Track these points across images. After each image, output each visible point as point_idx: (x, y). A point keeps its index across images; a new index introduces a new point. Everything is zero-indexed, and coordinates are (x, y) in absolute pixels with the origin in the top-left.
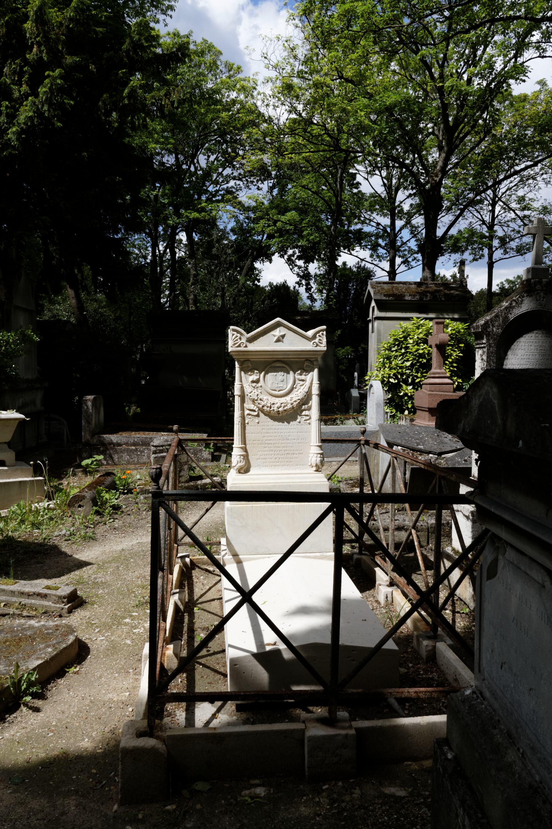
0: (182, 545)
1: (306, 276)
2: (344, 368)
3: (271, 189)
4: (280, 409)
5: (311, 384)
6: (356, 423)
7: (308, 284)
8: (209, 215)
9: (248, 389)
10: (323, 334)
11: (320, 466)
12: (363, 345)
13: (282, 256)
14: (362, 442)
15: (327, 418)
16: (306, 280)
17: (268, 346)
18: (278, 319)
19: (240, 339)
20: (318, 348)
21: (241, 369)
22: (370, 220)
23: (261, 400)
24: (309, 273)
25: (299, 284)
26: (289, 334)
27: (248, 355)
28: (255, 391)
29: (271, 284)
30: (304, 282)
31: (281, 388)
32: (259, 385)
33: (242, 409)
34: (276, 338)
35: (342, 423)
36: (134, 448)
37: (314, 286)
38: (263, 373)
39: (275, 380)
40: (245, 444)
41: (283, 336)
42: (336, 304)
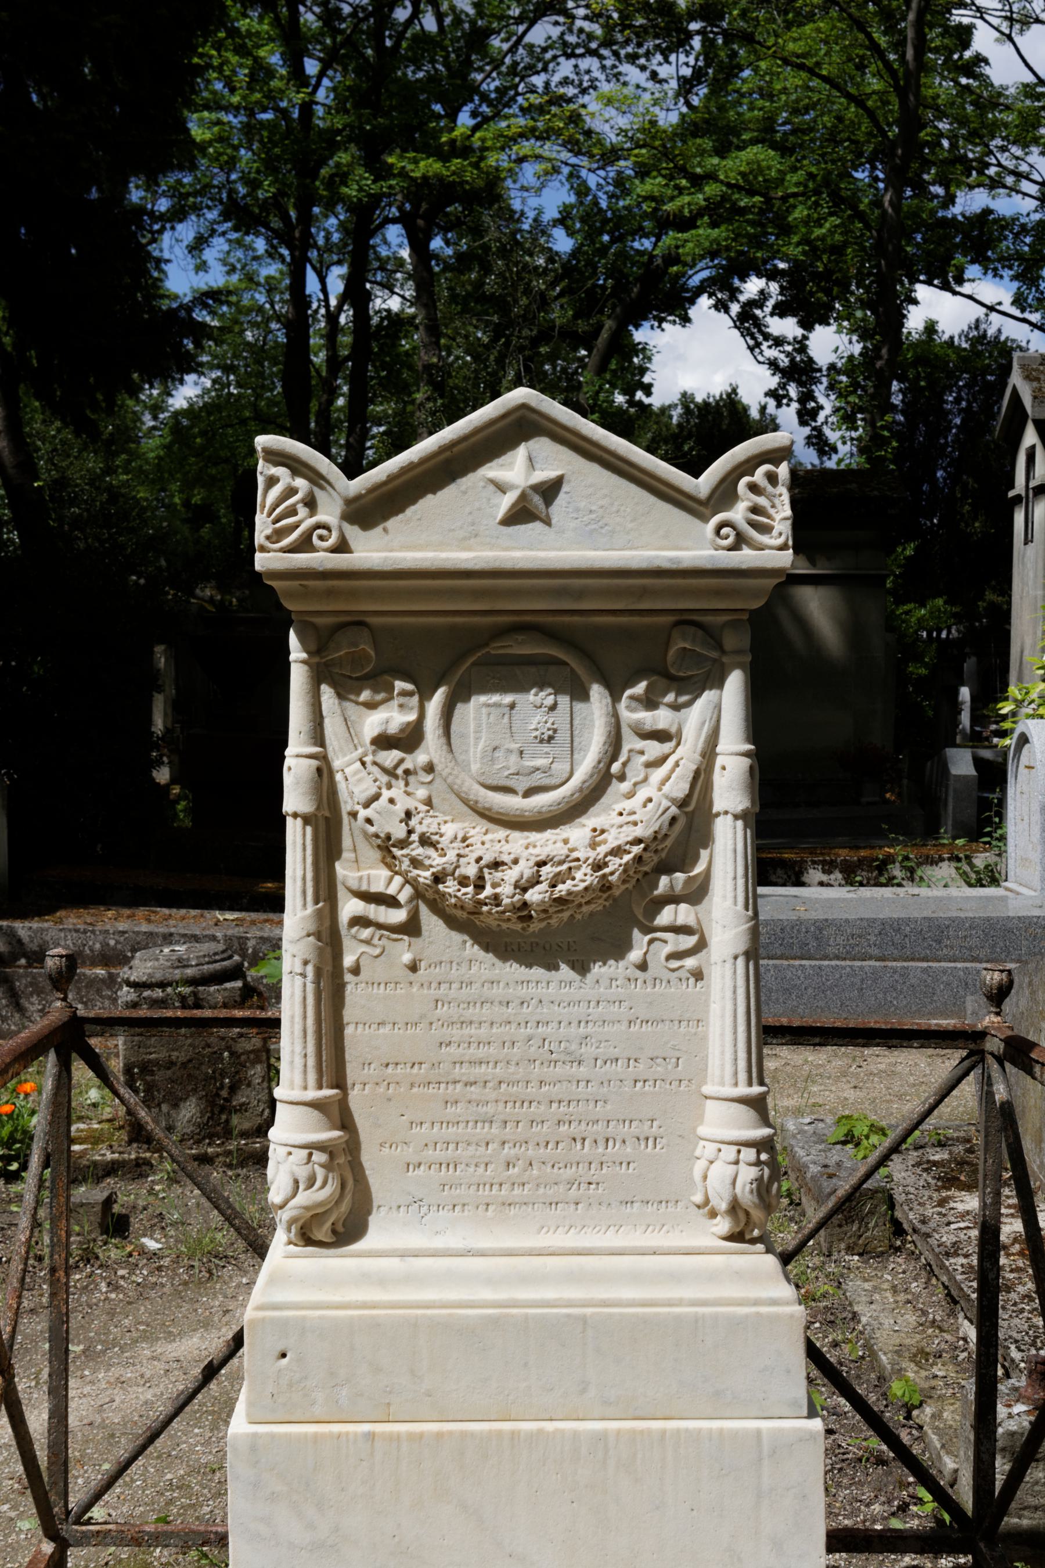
0: (84, 1540)
1: (799, 371)
2: (923, 671)
3: (686, 86)
4: (534, 896)
5: (709, 753)
6: (964, 875)
7: (806, 397)
8: (476, 166)
9: (354, 783)
10: (772, 478)
11: (757, 1214)
12: (990, 596)
13: (721, 306)
14: (994, 1045)
15: (853, 856)
16: (800, 383)
17: (463, 544)
18: (521, 394)
19: (311, 503)
20: (746, 558)
21: (321, 673)
22: (1019, 175)
23: (425, 841)
24: (811, 360)
25: (777, 396)
26: (586, 480)
27: (354, 594)
28: (397, 791)
29: (686, 398)
30: (793, 391)
31: (537, 779)
32: (421, 758)
33: (326, 889)
34: (507, 501)
35: (911, 875)
36: (101, 972)
37: (827, 403)
38: (440, 695)
39: (499, 730)
40: (340, 1082)
41: (550, 490)
42: (899, 457)
